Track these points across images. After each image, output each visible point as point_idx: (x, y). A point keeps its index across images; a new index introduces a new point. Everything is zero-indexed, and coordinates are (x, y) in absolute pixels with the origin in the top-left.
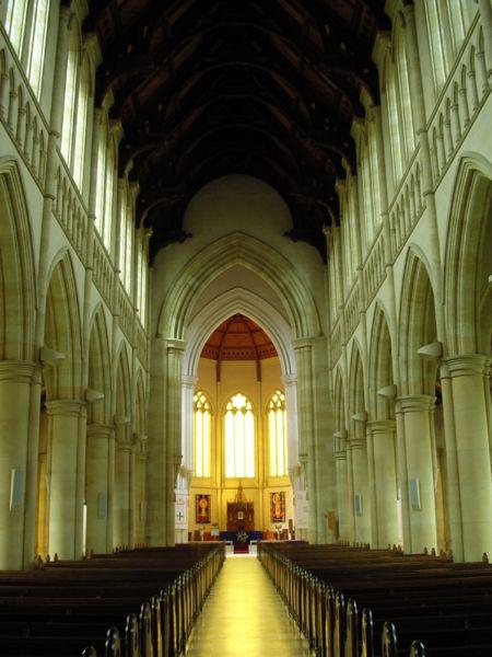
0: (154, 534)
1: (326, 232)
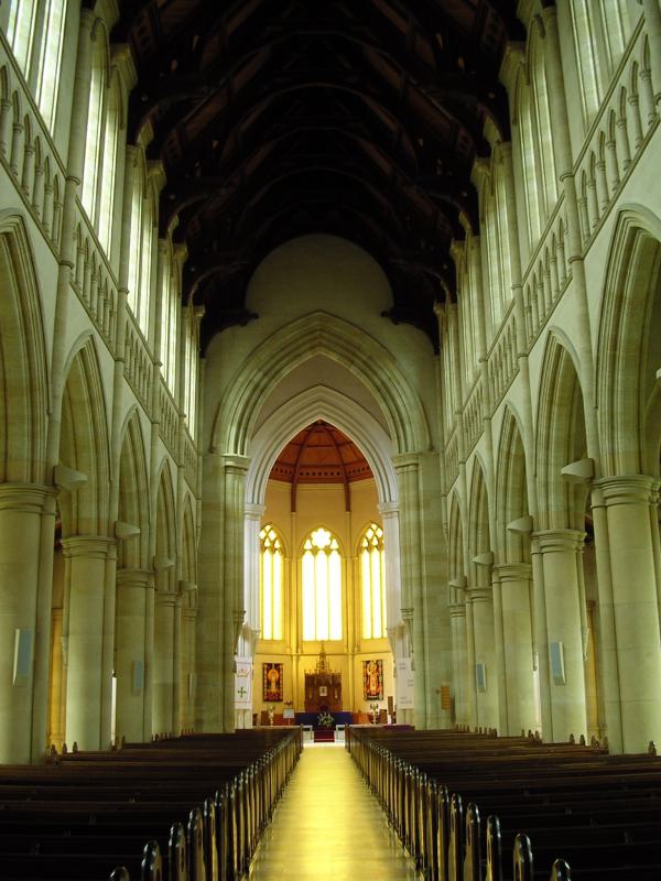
0: (206, 716)
1: (438, 311)
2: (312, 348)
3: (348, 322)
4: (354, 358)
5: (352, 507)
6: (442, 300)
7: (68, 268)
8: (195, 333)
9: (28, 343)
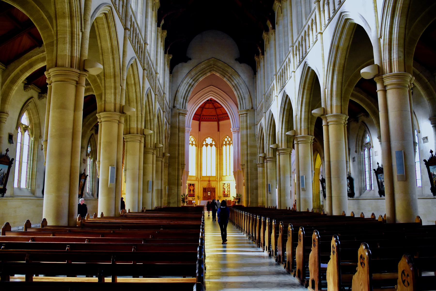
0: (172, 201)
1: (256, 59)
2: (210, 71)
4: (225, 75)
5: (220, 130)
6: (258, 55)
8: (168, 64)
9: (113, 59)
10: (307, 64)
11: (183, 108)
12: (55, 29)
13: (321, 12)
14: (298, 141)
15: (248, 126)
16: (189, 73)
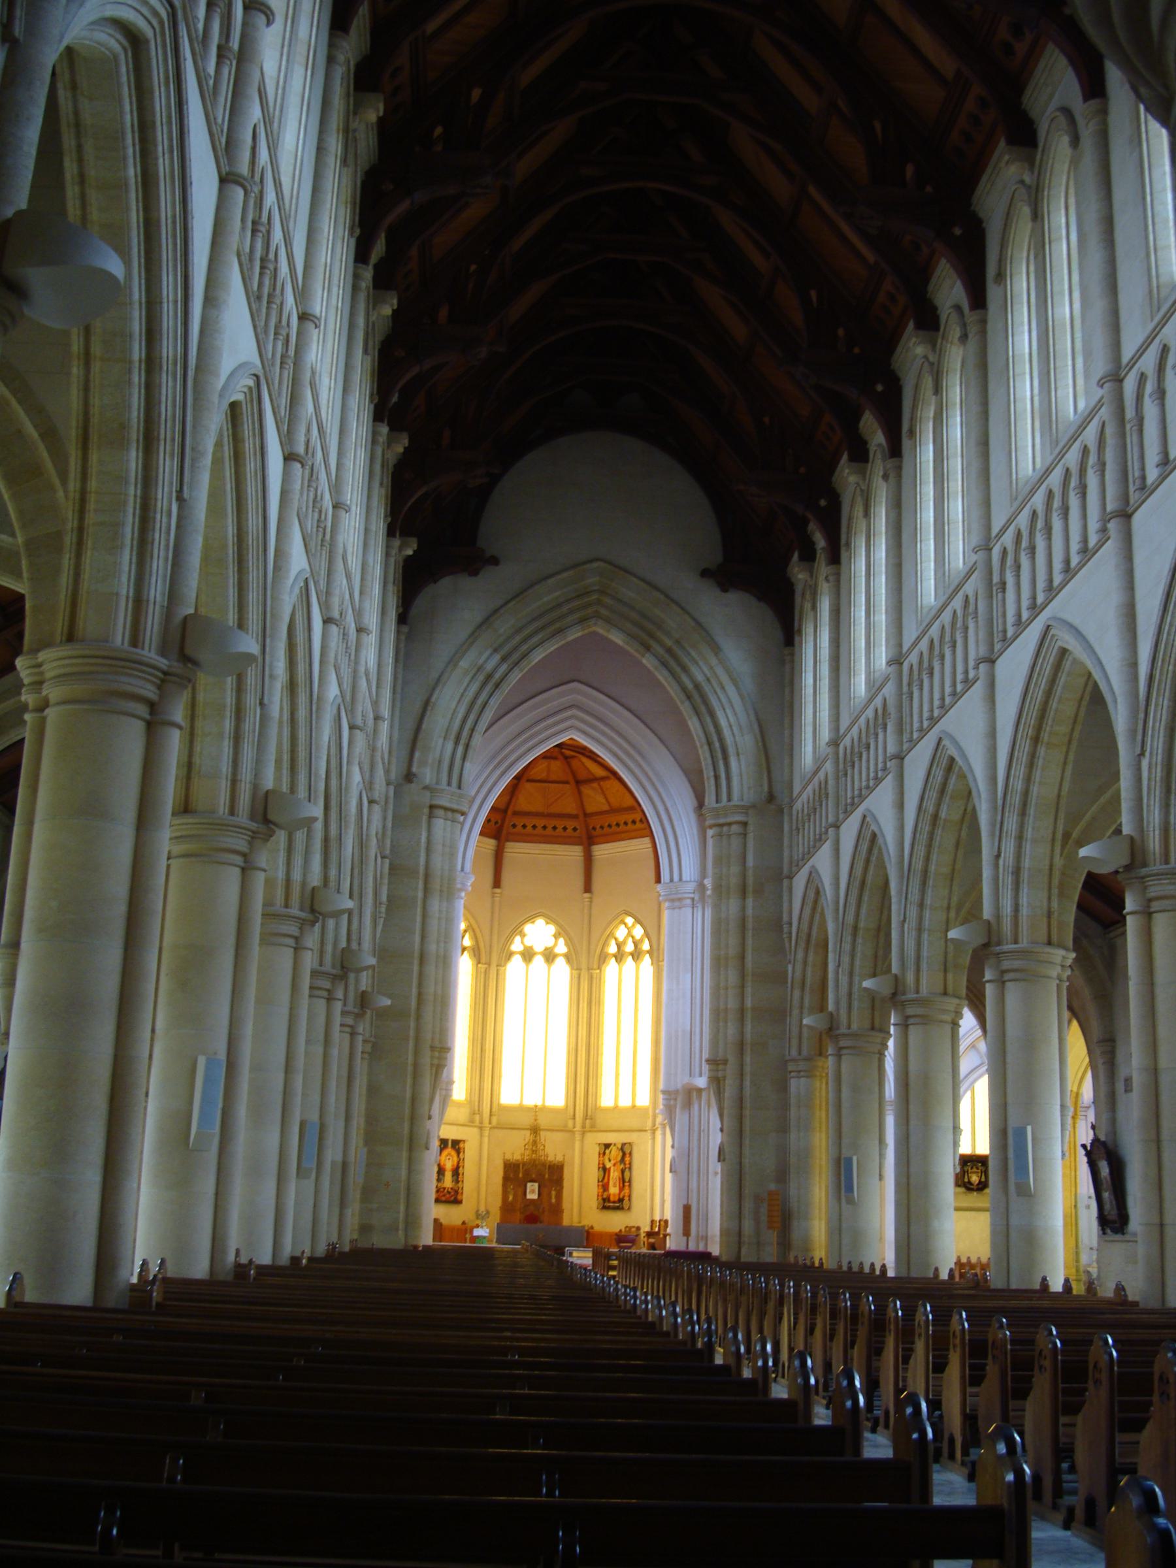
2: (582, 621)
3: (643, 580)
4: (652, 643)
7: (299, 465)
10: (1053, 636)
11: (449, 784)
12: (73, 485)
13: (1128, 427)
14: (1003, 972)
15: (750, 881)
16: (486, 622)
